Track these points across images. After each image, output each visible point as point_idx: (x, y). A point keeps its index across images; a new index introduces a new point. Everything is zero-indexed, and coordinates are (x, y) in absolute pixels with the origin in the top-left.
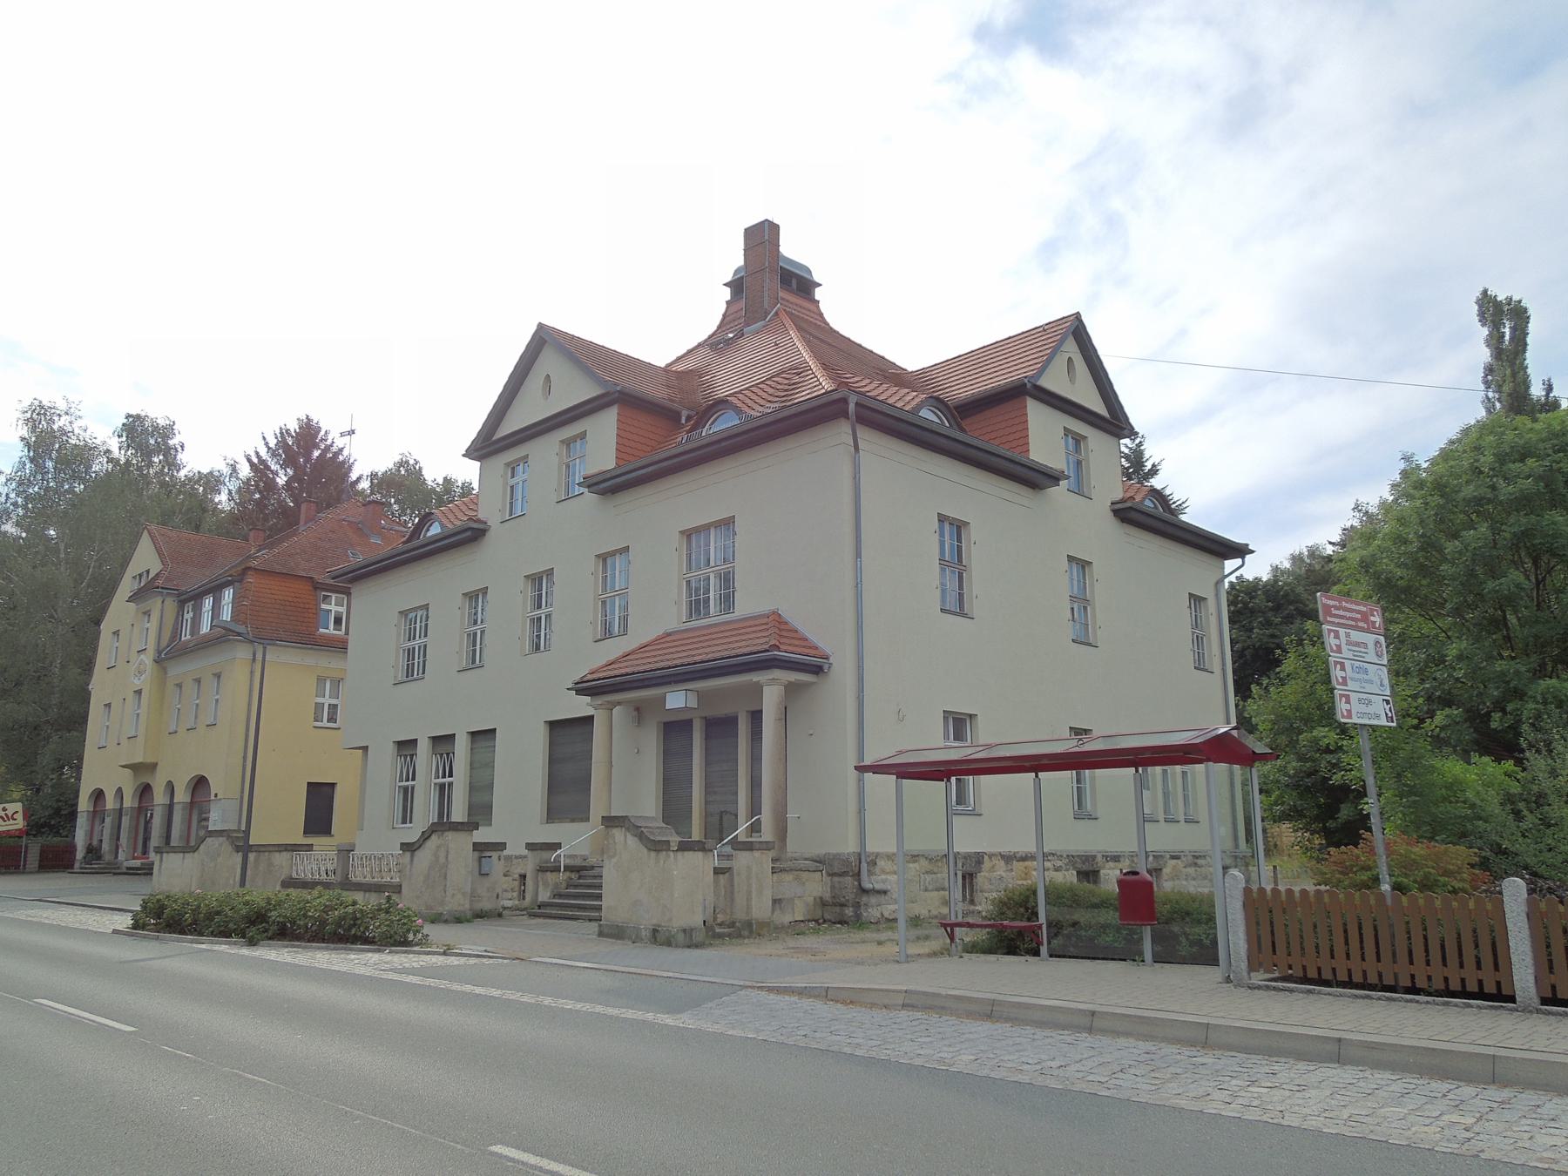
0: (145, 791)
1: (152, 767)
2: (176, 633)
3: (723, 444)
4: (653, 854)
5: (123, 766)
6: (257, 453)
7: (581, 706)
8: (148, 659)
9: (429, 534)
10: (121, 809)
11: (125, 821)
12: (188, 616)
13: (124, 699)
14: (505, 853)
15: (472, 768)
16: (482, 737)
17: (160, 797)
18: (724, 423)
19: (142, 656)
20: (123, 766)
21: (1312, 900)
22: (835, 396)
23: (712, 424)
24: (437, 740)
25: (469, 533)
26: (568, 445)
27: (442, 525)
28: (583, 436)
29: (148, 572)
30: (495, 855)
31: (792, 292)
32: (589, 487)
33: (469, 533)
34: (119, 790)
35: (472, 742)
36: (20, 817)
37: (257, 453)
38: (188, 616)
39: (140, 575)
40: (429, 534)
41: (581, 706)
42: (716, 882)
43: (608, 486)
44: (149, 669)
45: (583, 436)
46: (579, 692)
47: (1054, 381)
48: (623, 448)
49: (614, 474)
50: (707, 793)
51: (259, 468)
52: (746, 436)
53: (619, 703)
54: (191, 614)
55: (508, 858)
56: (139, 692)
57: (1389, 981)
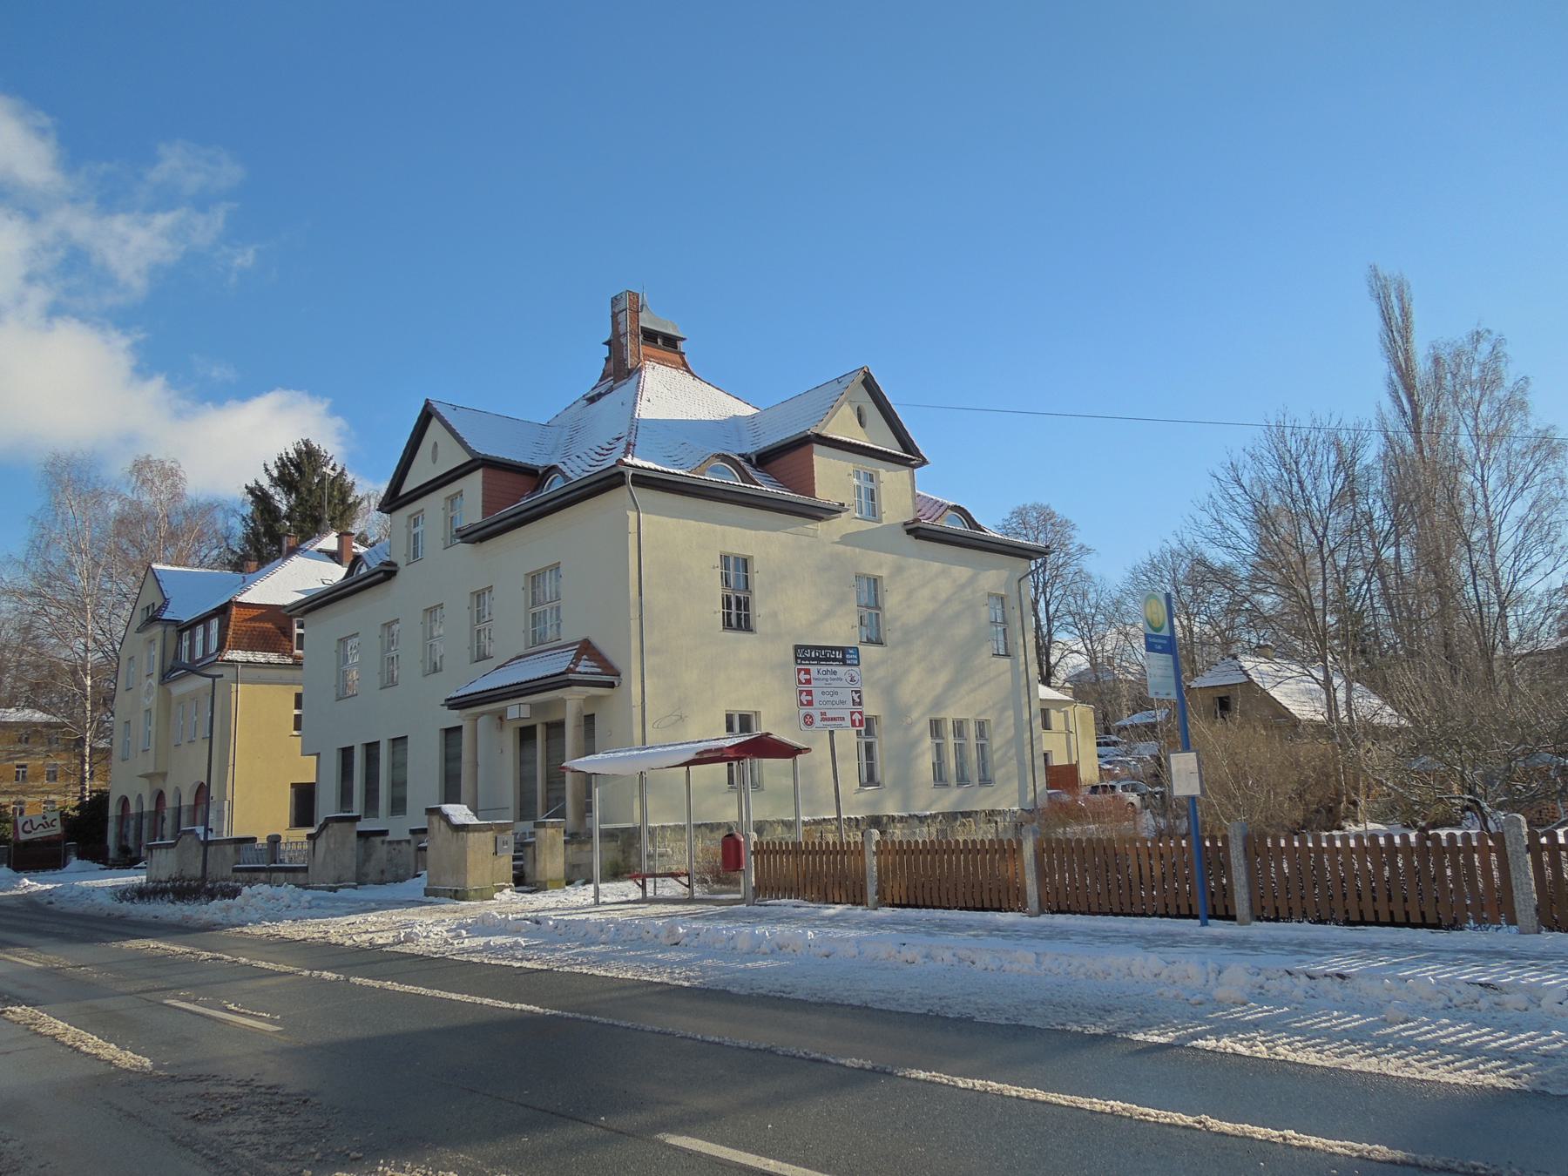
0: (160, 797)
1: (164, 775)
2: (177, 656)
3: (548, 505)
4: (455, 834)
5: (140, 776)
6: (287, 453)
7: (454, 718)
8: (154, 681)
9: (361, 572)
10: (180, 808)
11: (145, 823)
12: (186, 644)
13: (128, 722)
14: (388, 838)
15: (447, 760)
16: (399, 742)
17: (170, 802)
18: (555, 485)
19: (150, 680)
20: (140, 776)
21: (1445, 844)
22: (614, 471)
23: (550, 484)
24: (368, 746)
25: (381, 575)
26: (452, 501)
27: (368, 567)
28: (460, 493)
29: (153, 604)
30: (378, 840)
31: (659, 348)
32: (462, 537)
33: (381, 575)
34: (140, 796)
35: (393, 747)
36: (58, 824)
37: (287, 453)
38: (186, 644)
39: (148, 608)
40: (361, 572)
41: (454, 718)
42: (565, 849)
43: (477, 535)
44: (155, 690)
45: (460, 493)
46: (452, 707)
47: (843, 427)
48: (488, 506)
49: (480, 526)
50: (548, 783)
51: (259, 497)
52: (598, 485)
53: (483, 714)
54: (188, 643)
55: (390, 843)
56: (148, 711)
57: (970, 904)
